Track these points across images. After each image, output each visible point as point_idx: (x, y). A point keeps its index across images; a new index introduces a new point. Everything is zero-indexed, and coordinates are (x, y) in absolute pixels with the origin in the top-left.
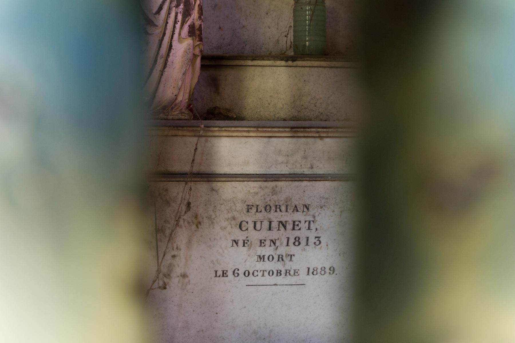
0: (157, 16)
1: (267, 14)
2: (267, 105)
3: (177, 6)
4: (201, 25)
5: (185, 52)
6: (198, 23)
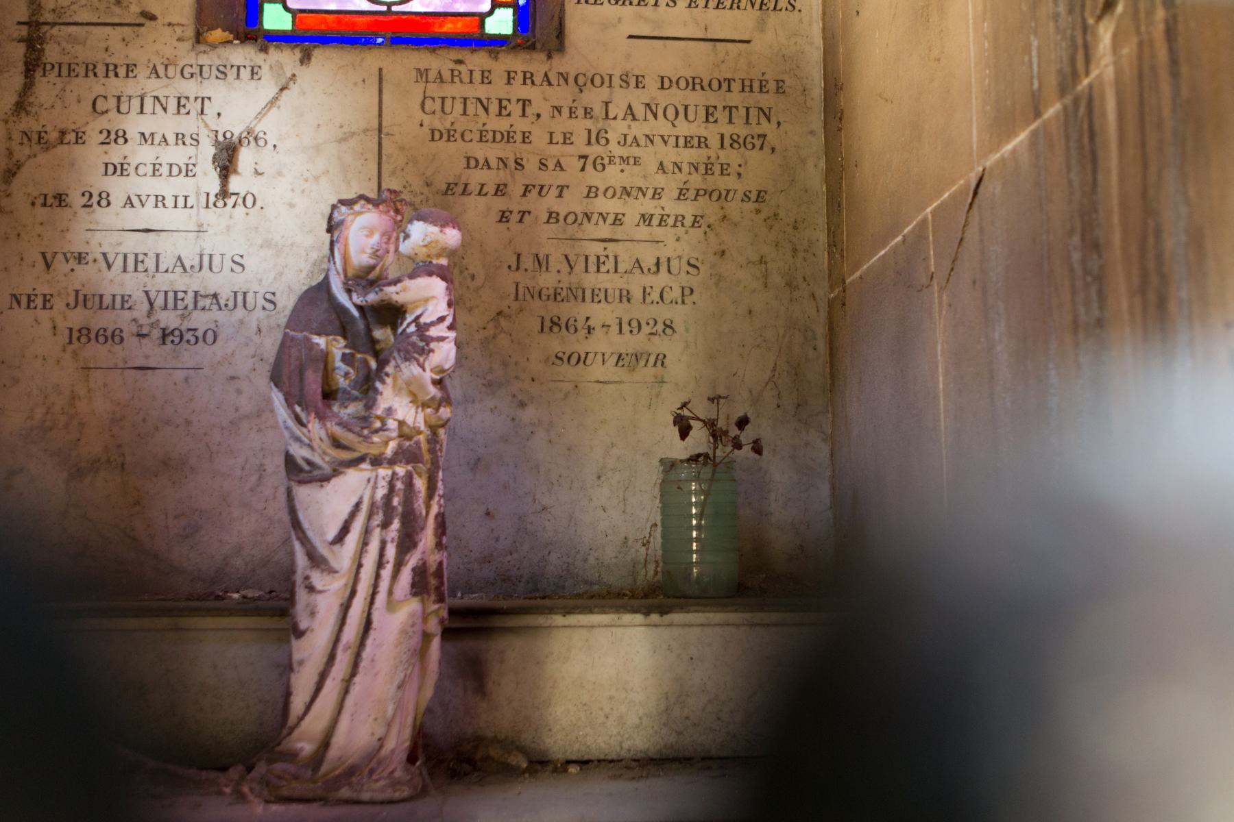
0: (336, 548)
1: (599, 478)
2: (601, 719)
3: (385, 525)
4: (441, 563)
5: (404, 632)
6: (434, 559)
